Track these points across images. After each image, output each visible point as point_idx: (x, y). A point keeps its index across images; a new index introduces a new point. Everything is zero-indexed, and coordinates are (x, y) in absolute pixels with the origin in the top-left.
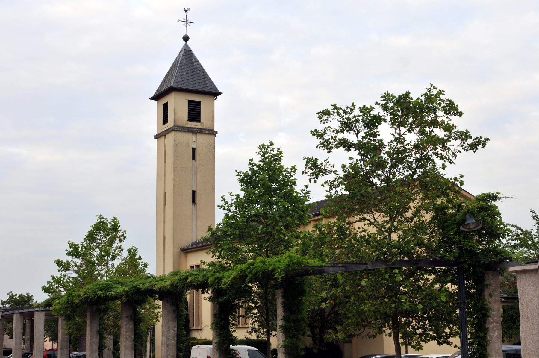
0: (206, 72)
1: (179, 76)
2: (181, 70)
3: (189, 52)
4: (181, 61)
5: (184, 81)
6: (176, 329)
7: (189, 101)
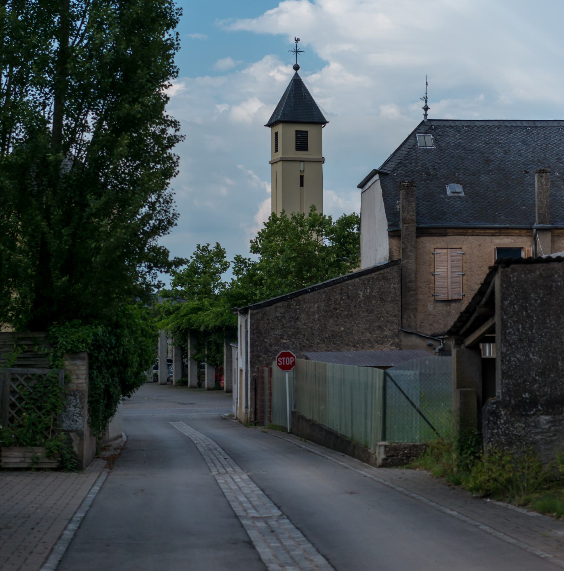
7: (297, 131)
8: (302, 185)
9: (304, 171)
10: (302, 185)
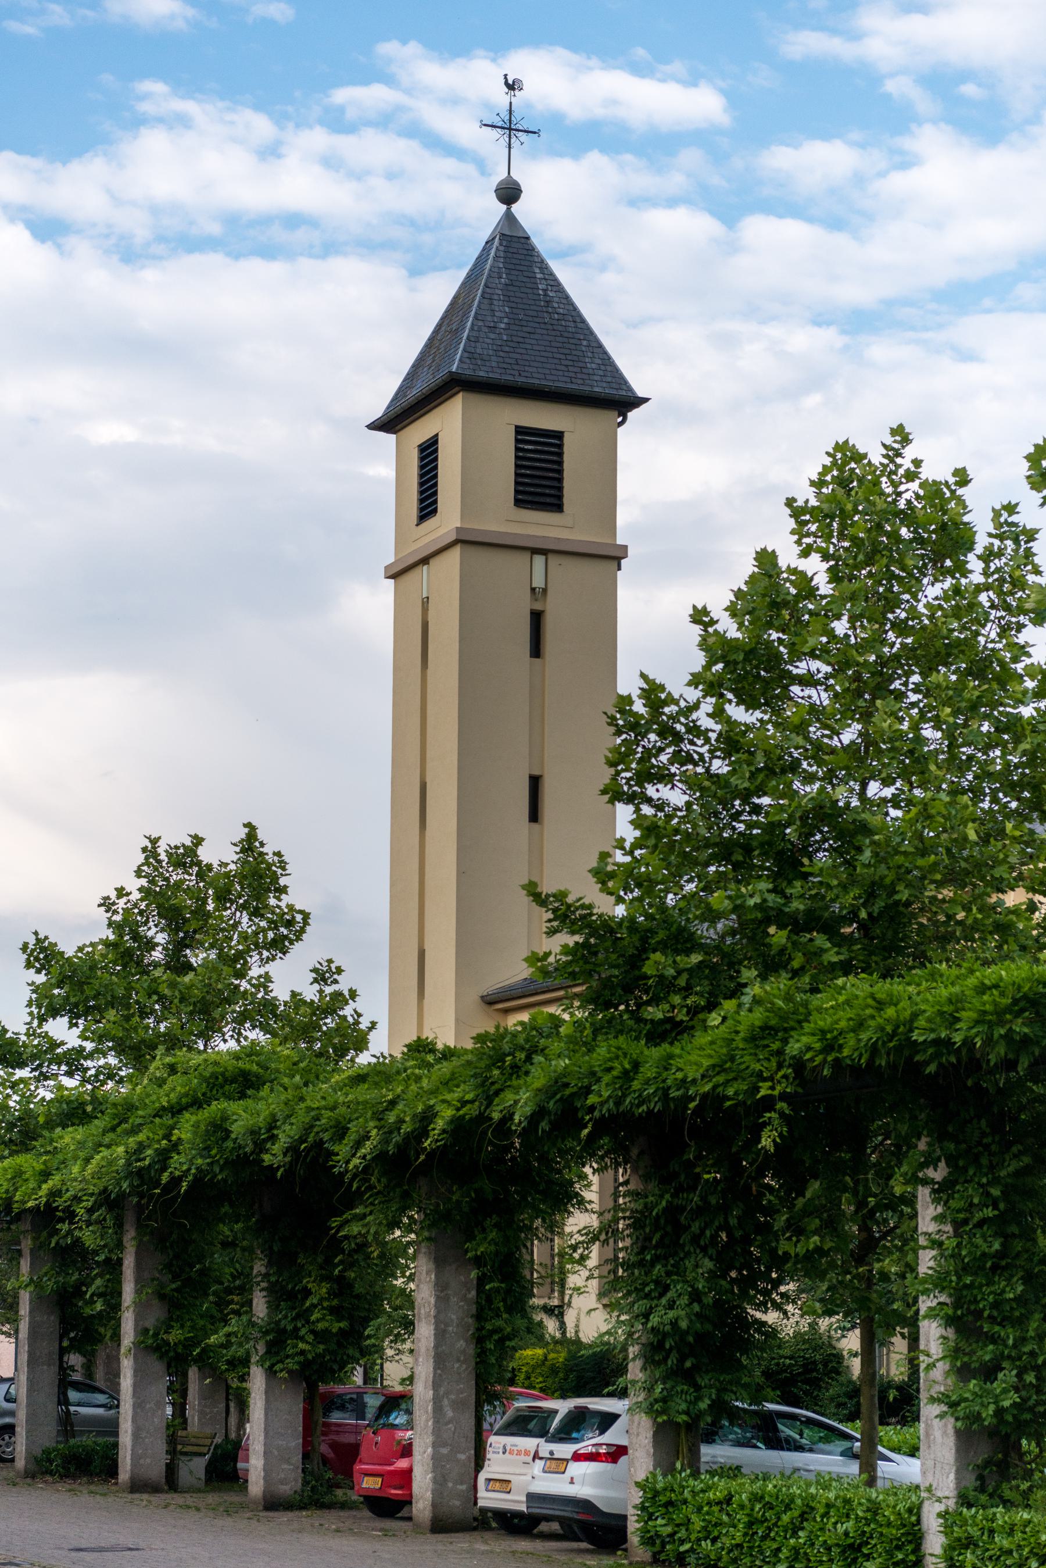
0: (583, 321)
1: (482, 335)
2: (488, 313)
3: (520, 246)
4: (489, 276)
5: (501, 354)
6: (474, 1293)
7: (520, 430)
8: (536, 650)
9: (545, 591)
10: (536, 650)
